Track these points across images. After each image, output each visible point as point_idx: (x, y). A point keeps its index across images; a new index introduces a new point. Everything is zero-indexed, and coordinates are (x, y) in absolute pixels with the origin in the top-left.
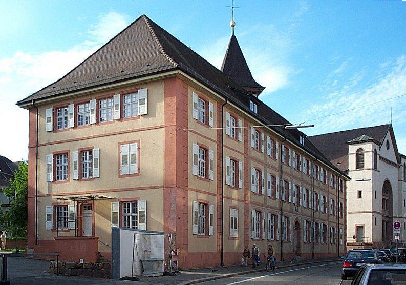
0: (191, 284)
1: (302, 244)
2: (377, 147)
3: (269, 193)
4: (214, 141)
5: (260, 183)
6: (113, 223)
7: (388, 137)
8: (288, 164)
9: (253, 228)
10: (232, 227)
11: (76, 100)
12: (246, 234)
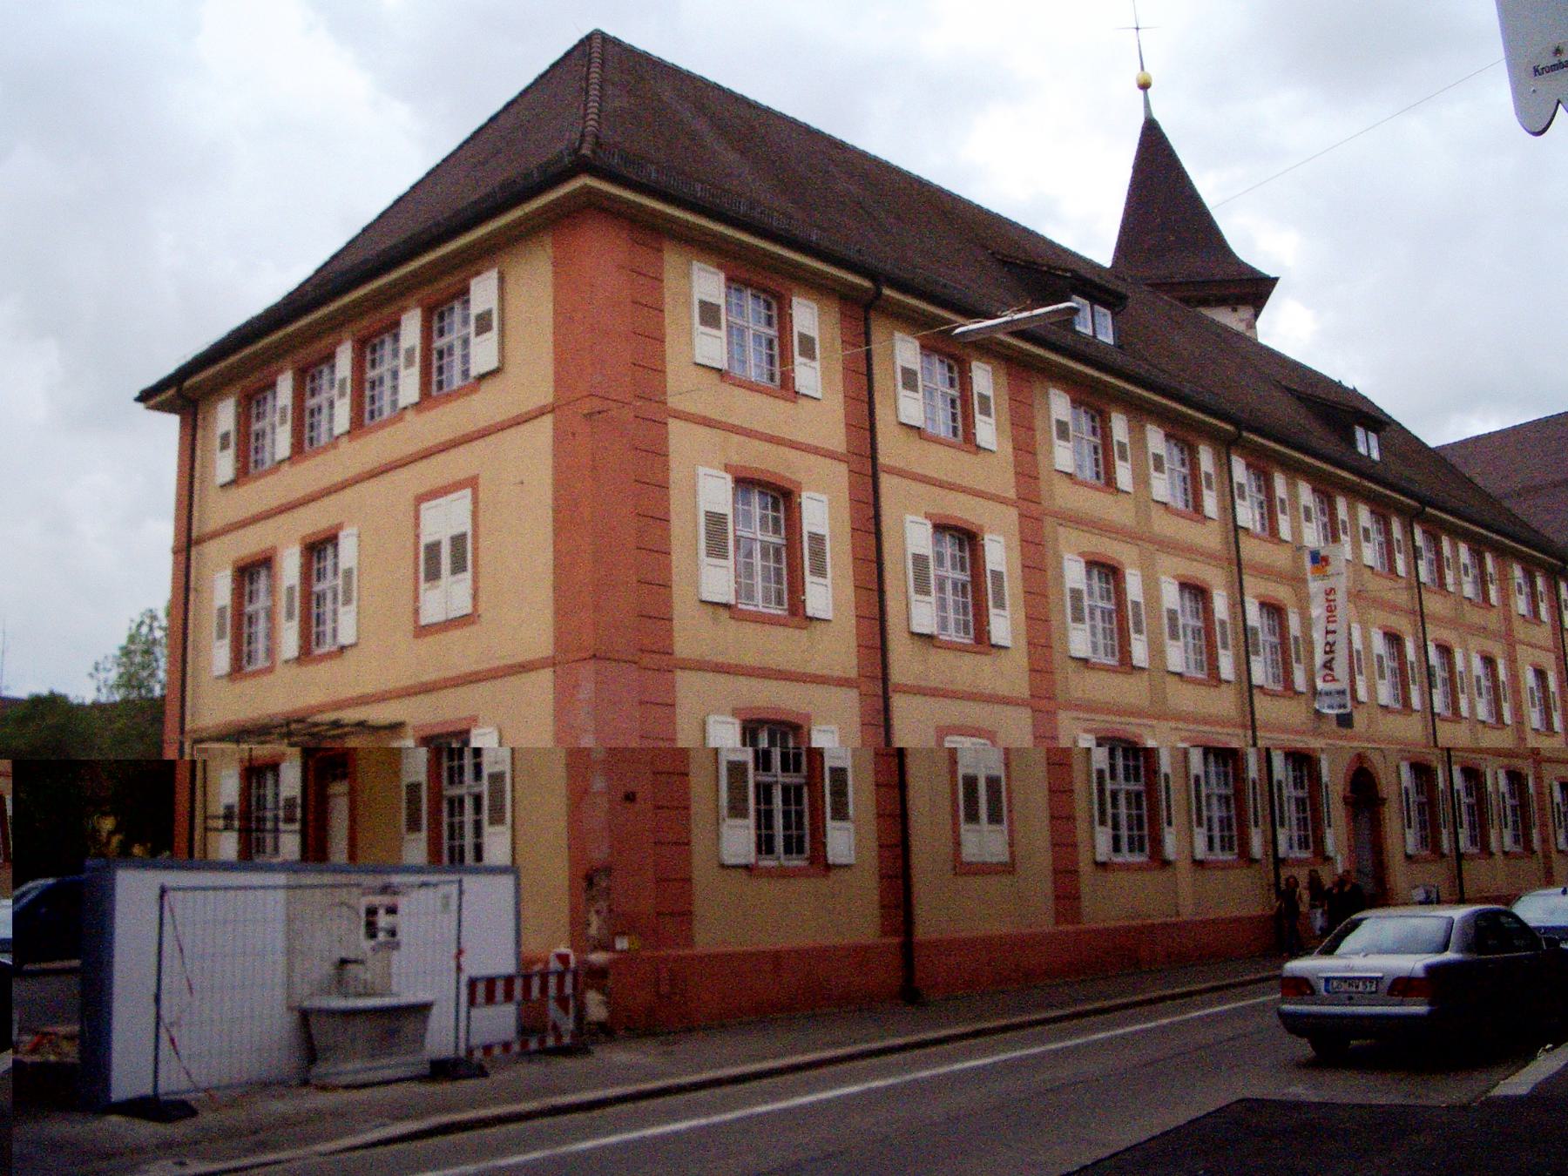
0: (229, 1171)
3: (1482, 711)
4: (831, 455)
5: (1122, 619)
8: (1442, 584)
10: (972, 817)
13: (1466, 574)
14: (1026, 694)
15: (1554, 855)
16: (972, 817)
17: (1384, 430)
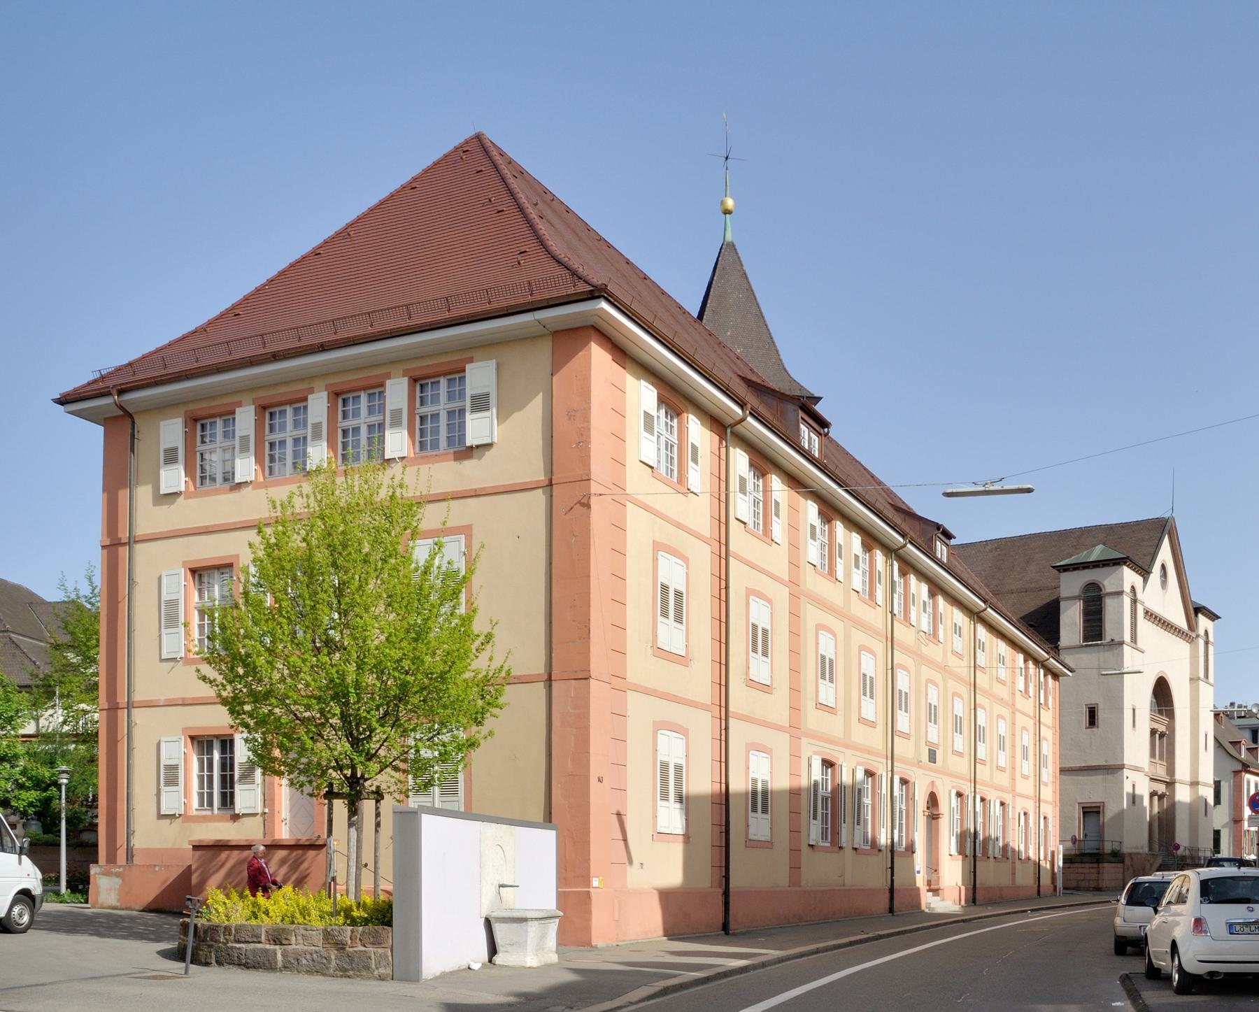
7: (1165, 554)
11: (262, 393)
13: (857, 566)
16: (754, 810)
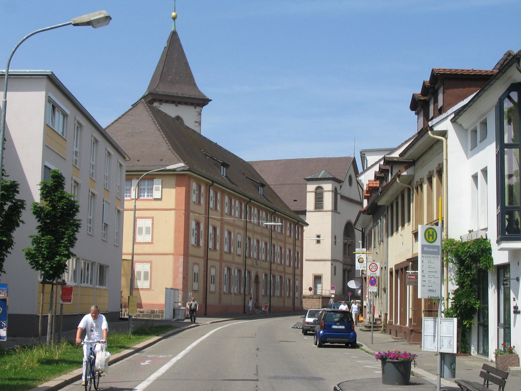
1: (260, 297)
2: (338, 185)
6: (100, 285)
9: (225, 283)
10: (212, 283)
12: (220, 289)
14: (219, 259)
15: (286, 297)
17: (264, 187)
